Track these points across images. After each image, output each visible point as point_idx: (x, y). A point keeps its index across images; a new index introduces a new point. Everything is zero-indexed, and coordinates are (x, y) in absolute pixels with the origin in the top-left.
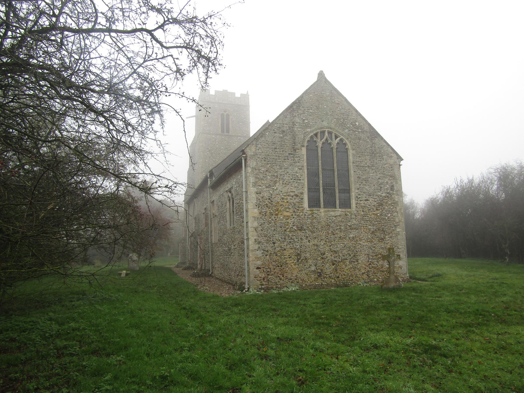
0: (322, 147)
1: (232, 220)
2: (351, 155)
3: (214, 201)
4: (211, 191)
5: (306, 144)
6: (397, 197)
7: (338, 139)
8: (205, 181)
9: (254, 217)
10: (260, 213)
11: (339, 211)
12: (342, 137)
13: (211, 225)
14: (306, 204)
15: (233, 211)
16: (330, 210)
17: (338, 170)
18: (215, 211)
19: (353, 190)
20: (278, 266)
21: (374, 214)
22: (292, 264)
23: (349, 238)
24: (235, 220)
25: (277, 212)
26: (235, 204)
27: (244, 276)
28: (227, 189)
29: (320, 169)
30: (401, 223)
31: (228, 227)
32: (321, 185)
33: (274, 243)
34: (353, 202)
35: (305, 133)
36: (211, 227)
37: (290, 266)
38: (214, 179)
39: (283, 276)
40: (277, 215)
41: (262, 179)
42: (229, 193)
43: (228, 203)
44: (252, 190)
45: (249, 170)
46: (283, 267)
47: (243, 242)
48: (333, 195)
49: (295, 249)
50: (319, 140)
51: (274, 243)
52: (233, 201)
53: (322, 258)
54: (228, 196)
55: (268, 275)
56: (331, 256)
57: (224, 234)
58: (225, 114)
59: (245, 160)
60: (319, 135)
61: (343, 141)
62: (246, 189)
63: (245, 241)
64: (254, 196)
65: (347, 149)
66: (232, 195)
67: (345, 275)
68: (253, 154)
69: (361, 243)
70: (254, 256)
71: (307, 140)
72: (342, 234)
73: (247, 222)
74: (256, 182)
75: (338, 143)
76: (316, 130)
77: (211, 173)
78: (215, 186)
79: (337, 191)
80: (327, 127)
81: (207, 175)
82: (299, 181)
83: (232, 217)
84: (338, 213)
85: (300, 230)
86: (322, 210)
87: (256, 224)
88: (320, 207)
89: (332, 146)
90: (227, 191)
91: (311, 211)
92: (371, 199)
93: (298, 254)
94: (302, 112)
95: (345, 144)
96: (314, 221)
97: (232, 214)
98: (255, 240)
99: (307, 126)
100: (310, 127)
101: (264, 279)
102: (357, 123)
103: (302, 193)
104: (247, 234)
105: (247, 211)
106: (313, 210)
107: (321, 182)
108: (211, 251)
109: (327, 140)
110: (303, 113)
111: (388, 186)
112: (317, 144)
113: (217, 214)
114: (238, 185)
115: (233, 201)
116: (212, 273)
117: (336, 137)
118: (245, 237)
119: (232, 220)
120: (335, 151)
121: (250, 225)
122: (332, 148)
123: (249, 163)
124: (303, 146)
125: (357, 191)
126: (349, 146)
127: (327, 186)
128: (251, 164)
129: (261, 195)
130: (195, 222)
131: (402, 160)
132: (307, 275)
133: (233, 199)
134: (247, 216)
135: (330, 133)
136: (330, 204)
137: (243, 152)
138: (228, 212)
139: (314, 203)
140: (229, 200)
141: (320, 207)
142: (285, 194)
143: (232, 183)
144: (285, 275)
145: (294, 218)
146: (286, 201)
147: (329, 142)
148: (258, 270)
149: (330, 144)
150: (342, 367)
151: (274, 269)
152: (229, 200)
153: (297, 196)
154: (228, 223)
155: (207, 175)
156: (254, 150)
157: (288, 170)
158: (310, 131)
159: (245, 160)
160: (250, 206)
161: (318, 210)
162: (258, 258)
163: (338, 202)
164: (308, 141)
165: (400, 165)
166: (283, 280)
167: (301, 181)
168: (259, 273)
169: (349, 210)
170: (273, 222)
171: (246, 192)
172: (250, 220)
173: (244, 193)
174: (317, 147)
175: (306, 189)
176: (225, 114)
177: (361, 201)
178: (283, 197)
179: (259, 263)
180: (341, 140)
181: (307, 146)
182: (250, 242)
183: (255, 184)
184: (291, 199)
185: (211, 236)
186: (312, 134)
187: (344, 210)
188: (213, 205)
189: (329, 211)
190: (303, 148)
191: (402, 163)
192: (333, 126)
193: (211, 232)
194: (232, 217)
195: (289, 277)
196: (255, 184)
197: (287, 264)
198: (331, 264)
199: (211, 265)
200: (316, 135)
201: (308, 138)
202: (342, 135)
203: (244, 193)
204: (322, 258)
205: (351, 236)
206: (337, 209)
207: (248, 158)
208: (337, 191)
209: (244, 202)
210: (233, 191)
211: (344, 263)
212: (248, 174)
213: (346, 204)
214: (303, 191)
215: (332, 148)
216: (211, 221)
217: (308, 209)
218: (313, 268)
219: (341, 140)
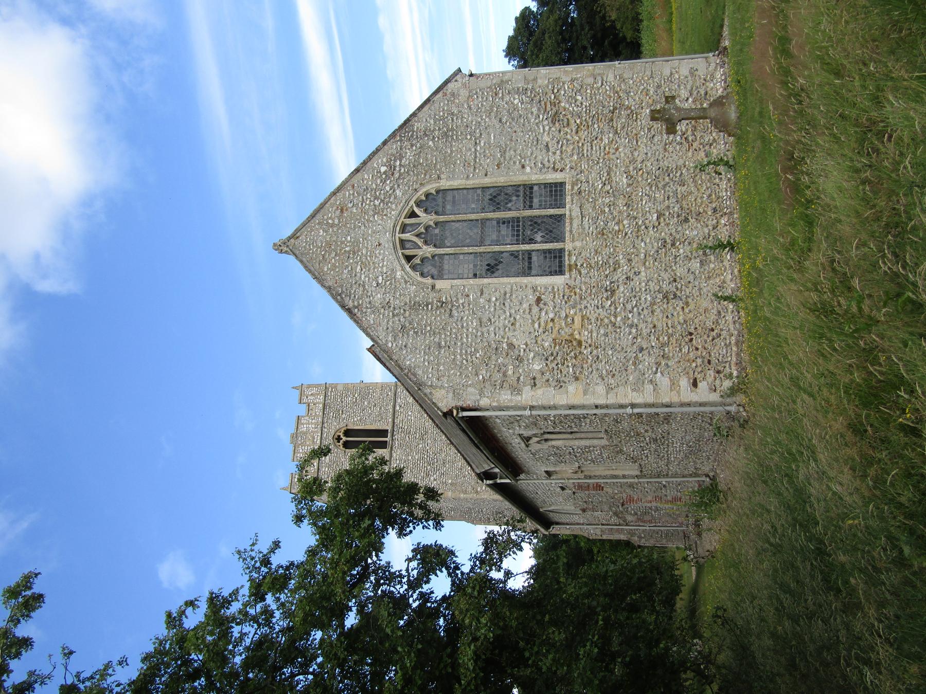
0: (435, 246)
1: (590, 435)
2: (451, 183)
3: (547, 472)
4: (522, 476)
5: (429, 281)
6: (540, 81)
7: (416, 210)
8: (499, 488)
9: (585, 392)
10: (577, 379)
11: (571, 208)
12: (412, 202)
13: (600, 477)
14: (558, 280)
15: (572, 433)
16: (568, 229)
17: (483, 210)
18: (567, 469)
19: (525, 178)
20: (691, 340)
21: (577, 132)
22: (687, 310)
23: (629, 185)
24: (591, 429)
25: (575, 343)
26: (557, 430)
27: (712, 413)
28: (523, 445)
29: (482, 249)
30: (597, 71)
31: (604, 442)
32: (515, 248)
33: (641, 349)
34: (553, 177)
35: (406, 282)
36: (605, 477)
37: (691, 315)
38: (497, 470)
39: (713, 330)
40: (580, 343)
41: (505, 375)
42: (531, 442)
43: (553, 443)
44: (528, 396)
45: (484, 402)
46: (692, 330)
47: (640, 415)
48: (535, 223)
49: (653, 304)
50: (420, 253)
51: (641, 349)
52: (549, 433)
53: (673, 245)
54: (538, 442)
55: (709, 362)
56: (668, 225)
57: (621, 451)
58: (344, 439)
59: (464, 409)
60: (408, 252)
61: (421, 201)
62: (525, 409)
63: (636, 411)
64: (540, 392)
65: (438, 192)
66: (535, 435)
67: (710, 195)
68: (451, 395)
69: (639, 159)
70: (670, 388)
71: (420, 279)
72: (621, 202)
73: (597, 407)
74: (511, 387)
75: (426, 211)
76: (398, 258)
77: (486, 476)
78: (514, 468)
79: (528, 213)
80: (394, 235)
81: (488, 485)
82: (508, 296)
83: (583, 435)
84: (576, 212)
85: (613, 292)
86: (568, 246)
87: (601, 389)
88: (562, 251)
89: (431, 223)
90: (527, 446)
91: (570, 270)
92: (546, 138)
93: (665, 297)
94: (361, 289)
95: (427, 195)
96: (592, 262)
97: (578, 435)
98: (633, 390)
99: (391, 276)
100: (393, 271)
101: (718, 372)
102: (383, 169)
103: (534, 289)
104: (622, 406)
105: (572, 407)
106: (570, 266)
107: (509, 248)
108: (659, 477)
109: (418, 236)
110: (364, 286)
111: (516, 102)
112: (429, 256)
113: (577, 465)
114: (516, 424)
115: (549, 433)
116: (707, 476)
117: (413, 215)
118: (629, 410)
119: (590, 435)
120: (442, 218)
121: (601, 401)
122: (436, 224)
123: (470, 403)
124: (433, 287)
125: (528, 169)
126: (431, 187)
127: (518, 236)
128: (473, 398)
129: (538, 376)
130: (593, 510)
131: (459, 70)
132: (709, 277)
133: (545, 433)
134: (583, 407)
135: (404, 229)
136: (553, 227)
137: (448, 414)
138: (572, 443)
139: (556, 263)
140: (546, 440)
141: (562, 251)
142: (536, 325)
143: (511, 437)
144: (709, 324)
145: (586, 307)
146: (551, 324)
147: (423, 230)
148: (700, 385)
149: (427, 228)
150: (834, 291)
151: (697, 349)
152: (546, 440)
153: (539, 300)
154: (596, 442)
155: (488, 485)
156: (443, 392)
157: (484, 320)
158: (402, 271)
159: (464, 409)
160: (562, 399)
161: (570, 255)
162: (674, 384)
163: (552, 211)
164: (422, 275)
165: (471, 75)
166: (721, 330)
167: (508, 290)
168: (705, 383)
169: (568, 187)
170: (595, 352)
171: (532, 408)
172: (590, 400)
173: (534, 413)
174: (433, 257)
175: (525, 280)
176: (344, 439)
177: (549, 161)
178: (541, 330)
179: (684, 383)
180: (419, 204)
181: (433, 277)
182: (639, 400)
183: (516, 390)
184: (546, 313)
185: (624, 477)
186: (407, 267)
187: (568, 199)
188: (556, 472)
189: (571, 231)
190: (437, 287)
191: (465, 71)
192: (390, 224)
193: (616, 477)
194: (583, 435)
195: (713, 317)
196: (516, 390)
197: (685, 322)
198: (686, 226)
199: (691, 479)
200: (409, 258)
201: (416, 276)
202: (407, 202)
203: (534, 413)
204: (673, 245)
205: (625, 181)
206: (568, 213)
207: (460, 404)
208: (528, 213)
209: (553, 413)
210: (527, 433)
211: (684, 197)
212: (495, 404)
213: (556, 191)
214: (530, 286)
215: (436, 224)
216: (590, 477)
217: (567, 276)
218: (695, 265)
219: (419, 204)
